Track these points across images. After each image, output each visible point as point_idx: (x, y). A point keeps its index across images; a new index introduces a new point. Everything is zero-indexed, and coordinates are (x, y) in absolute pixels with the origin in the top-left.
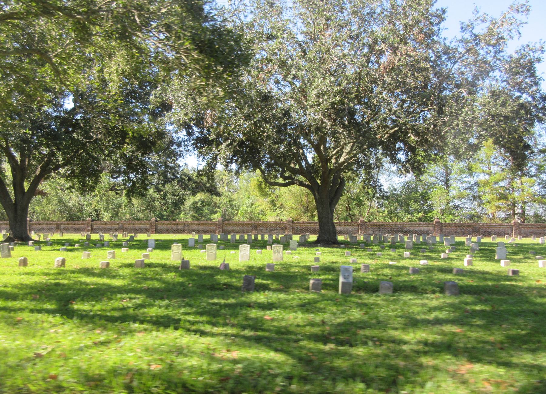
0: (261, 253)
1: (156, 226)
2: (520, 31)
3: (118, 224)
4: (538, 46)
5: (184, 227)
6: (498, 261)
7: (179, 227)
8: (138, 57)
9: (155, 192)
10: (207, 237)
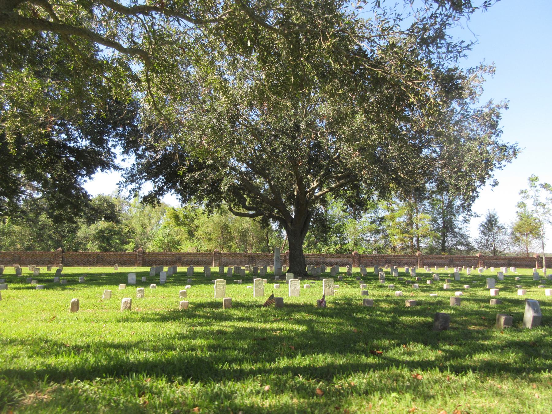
0: (279, 287)
1: (62, 257)
2: (482, 86)
3: (13, 255)
4: (503, 104)
5: (98, 259)
6: (489, 290)
7: (91, 259)
8: (347, 66)
9: (47, 218)
10: (215, 269)
